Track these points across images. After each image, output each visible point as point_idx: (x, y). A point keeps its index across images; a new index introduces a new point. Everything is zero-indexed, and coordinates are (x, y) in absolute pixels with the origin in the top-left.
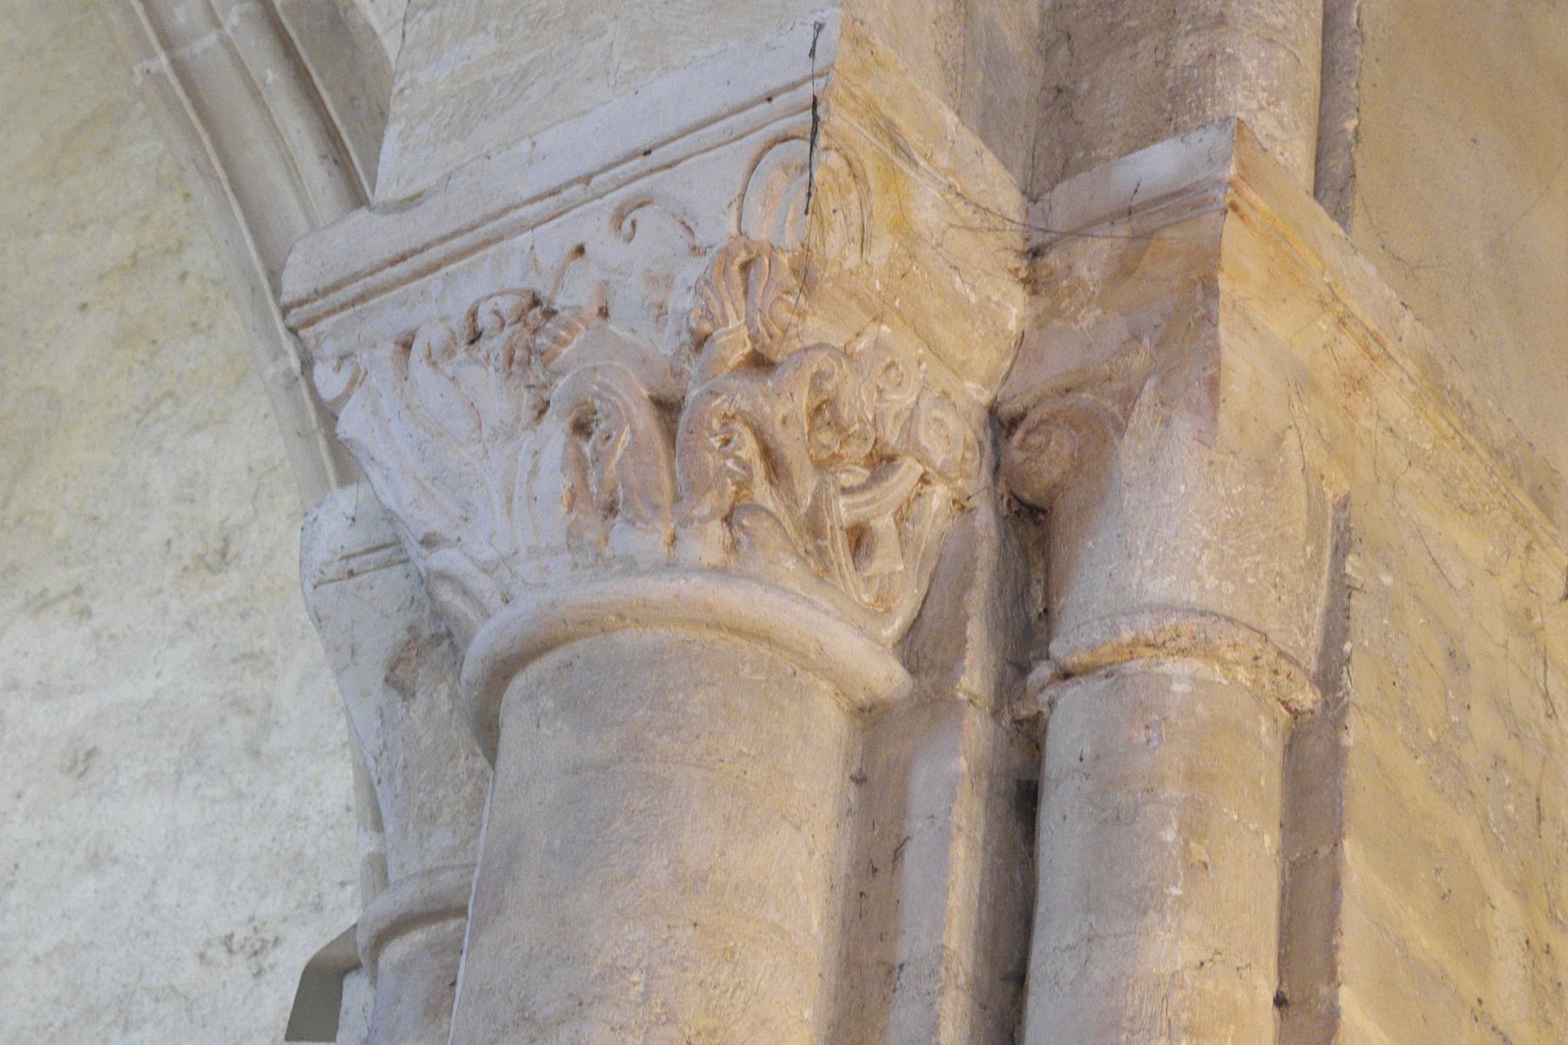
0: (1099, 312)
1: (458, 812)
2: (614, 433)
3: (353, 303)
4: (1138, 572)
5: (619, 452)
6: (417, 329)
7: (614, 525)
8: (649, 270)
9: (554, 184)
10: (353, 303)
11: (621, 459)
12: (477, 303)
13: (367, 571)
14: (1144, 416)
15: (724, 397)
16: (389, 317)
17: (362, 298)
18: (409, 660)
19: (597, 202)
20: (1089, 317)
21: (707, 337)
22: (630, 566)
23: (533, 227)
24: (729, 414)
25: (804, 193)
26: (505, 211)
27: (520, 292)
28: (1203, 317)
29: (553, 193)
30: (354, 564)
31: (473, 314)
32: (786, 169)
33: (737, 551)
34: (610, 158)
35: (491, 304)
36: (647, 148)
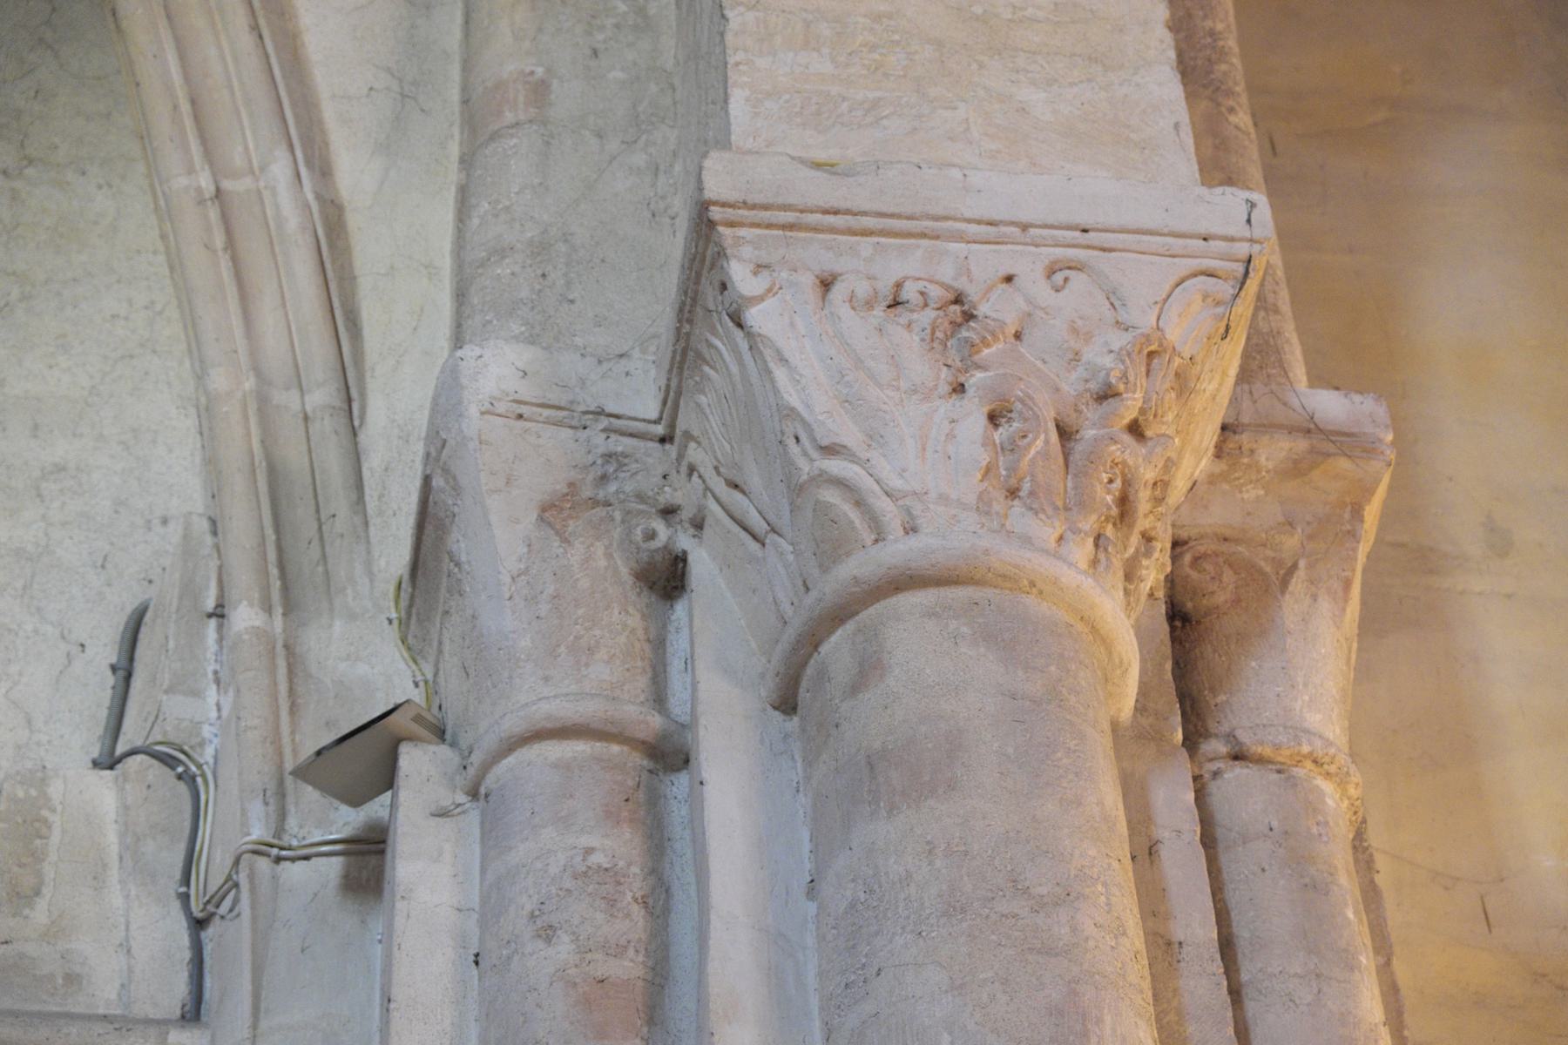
0: (1262, 492)
1: (614, 655)
2: (1030, 436)
3: (784, 227)
4: (1300, 702)
5: (1033, 452)
6: (841, 275)
7: (1013, 506)
8: (1073, 322)
9: (996, 217)
10: (784, 227)
11: (1034, 458)
12: (906, 278)
13: (538, 422)
14: (1300, 586)
15: (1119, 446)
16: (817, 254)
17: (791, 227)
18: (562, 509)
19: (1032, 249)
20: (1251, 493)
21: (1117, 395)
22: (1027, 541)
23: (969, 242)
24: (1116, 461)
25: (917, 275)
26: (946, 218)
27: (947, 287)
28: (1349, 532)
29: (990, 223)
30: (524, 409)
31: (899, 286)
32: (1205, 297)
33: (1095, 568)
34: (1050, 221)
35: (920, 285)
36: (1087, 227)
